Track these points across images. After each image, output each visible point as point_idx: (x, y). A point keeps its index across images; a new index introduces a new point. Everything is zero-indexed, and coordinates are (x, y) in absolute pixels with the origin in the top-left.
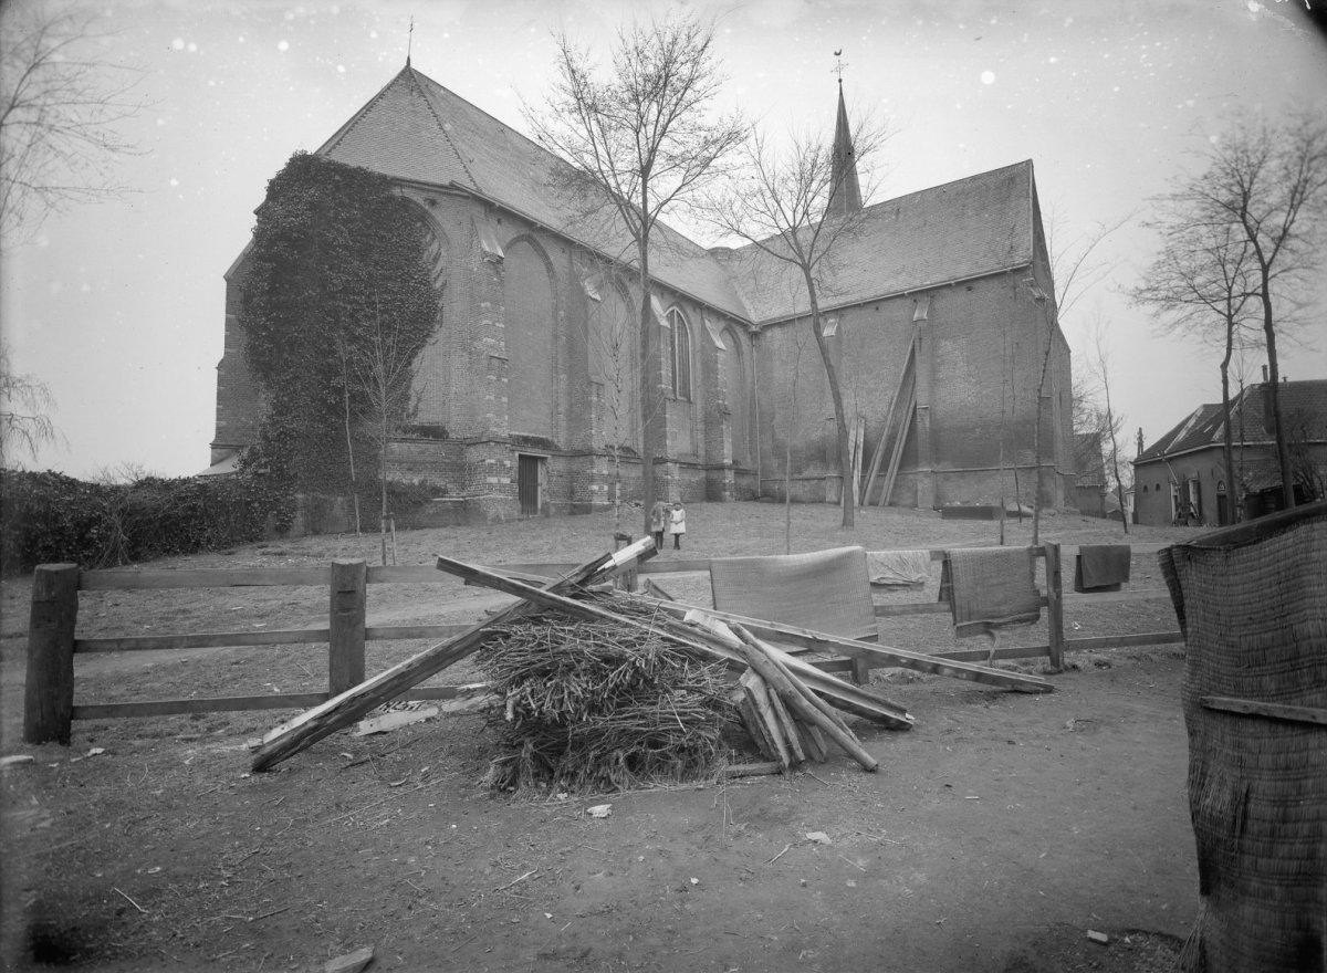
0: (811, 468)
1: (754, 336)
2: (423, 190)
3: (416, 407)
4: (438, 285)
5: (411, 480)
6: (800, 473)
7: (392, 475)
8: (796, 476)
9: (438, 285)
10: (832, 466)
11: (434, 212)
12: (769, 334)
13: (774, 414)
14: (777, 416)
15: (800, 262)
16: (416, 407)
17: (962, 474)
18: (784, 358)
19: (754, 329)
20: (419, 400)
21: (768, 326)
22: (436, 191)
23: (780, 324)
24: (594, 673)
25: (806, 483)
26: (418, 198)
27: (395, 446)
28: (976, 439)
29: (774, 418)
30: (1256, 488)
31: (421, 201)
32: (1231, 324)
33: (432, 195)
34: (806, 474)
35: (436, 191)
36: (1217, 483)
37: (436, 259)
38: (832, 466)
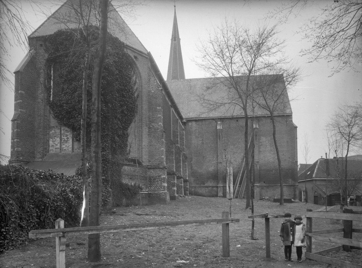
0: (209, 182)
1: (184, 124)
2: (133, 51)
3: (129, 150)
4: (136, 95)
5: (131, 183)
6: (204, 184)
7: (125, 181)
8: (202, 185)
9: (136, 95)
10: (221, 182)
11: (137, 62)
12: (190, 124)
13: (192, 158)
14: (193, 160)
15: (268, 110)
16: (129, 150)
17: (268, 187)
18: (197, 135)
19: (184, 121)
20: (130, 147)
21: (190, 120)
22: (137, 53)
23: (196, 121)
24: (212, 263)
25: (206, 188)
26: (132, 55)
27: (126, 168)
28: (273, 174)
29: (192, 160)
30: (328, 194)
31: (133, 57)
32: (349, 144)
33: (136, 55)
34: (206, 185)
35: (137, 53)
36: (314, 191)
37: (135, 84)
38: (221, 182)
